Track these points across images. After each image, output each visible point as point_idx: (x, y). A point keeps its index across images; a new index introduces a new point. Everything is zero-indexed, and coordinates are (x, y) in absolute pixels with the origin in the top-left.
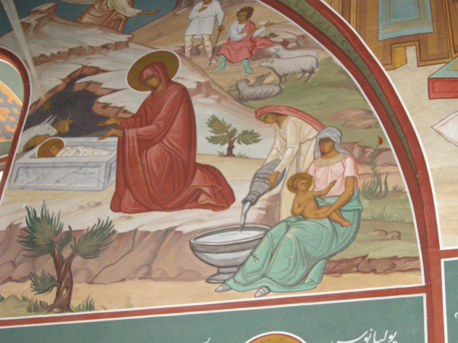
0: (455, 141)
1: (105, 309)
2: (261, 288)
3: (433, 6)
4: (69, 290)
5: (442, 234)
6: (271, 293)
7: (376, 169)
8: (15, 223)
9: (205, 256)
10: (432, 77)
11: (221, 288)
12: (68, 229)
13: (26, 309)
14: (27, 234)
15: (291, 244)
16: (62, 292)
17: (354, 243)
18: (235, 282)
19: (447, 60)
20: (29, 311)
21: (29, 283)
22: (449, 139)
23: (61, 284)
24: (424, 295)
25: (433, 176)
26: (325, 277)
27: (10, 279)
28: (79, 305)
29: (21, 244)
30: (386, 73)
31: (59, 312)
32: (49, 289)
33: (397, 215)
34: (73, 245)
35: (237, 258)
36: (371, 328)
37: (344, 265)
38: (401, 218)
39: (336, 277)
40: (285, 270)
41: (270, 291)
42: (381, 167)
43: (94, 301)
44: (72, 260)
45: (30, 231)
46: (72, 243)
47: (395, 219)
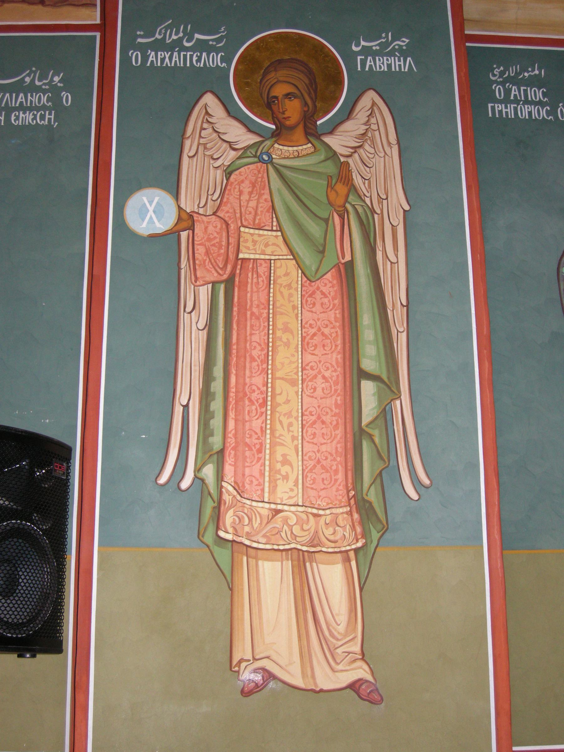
24: (98, 35)
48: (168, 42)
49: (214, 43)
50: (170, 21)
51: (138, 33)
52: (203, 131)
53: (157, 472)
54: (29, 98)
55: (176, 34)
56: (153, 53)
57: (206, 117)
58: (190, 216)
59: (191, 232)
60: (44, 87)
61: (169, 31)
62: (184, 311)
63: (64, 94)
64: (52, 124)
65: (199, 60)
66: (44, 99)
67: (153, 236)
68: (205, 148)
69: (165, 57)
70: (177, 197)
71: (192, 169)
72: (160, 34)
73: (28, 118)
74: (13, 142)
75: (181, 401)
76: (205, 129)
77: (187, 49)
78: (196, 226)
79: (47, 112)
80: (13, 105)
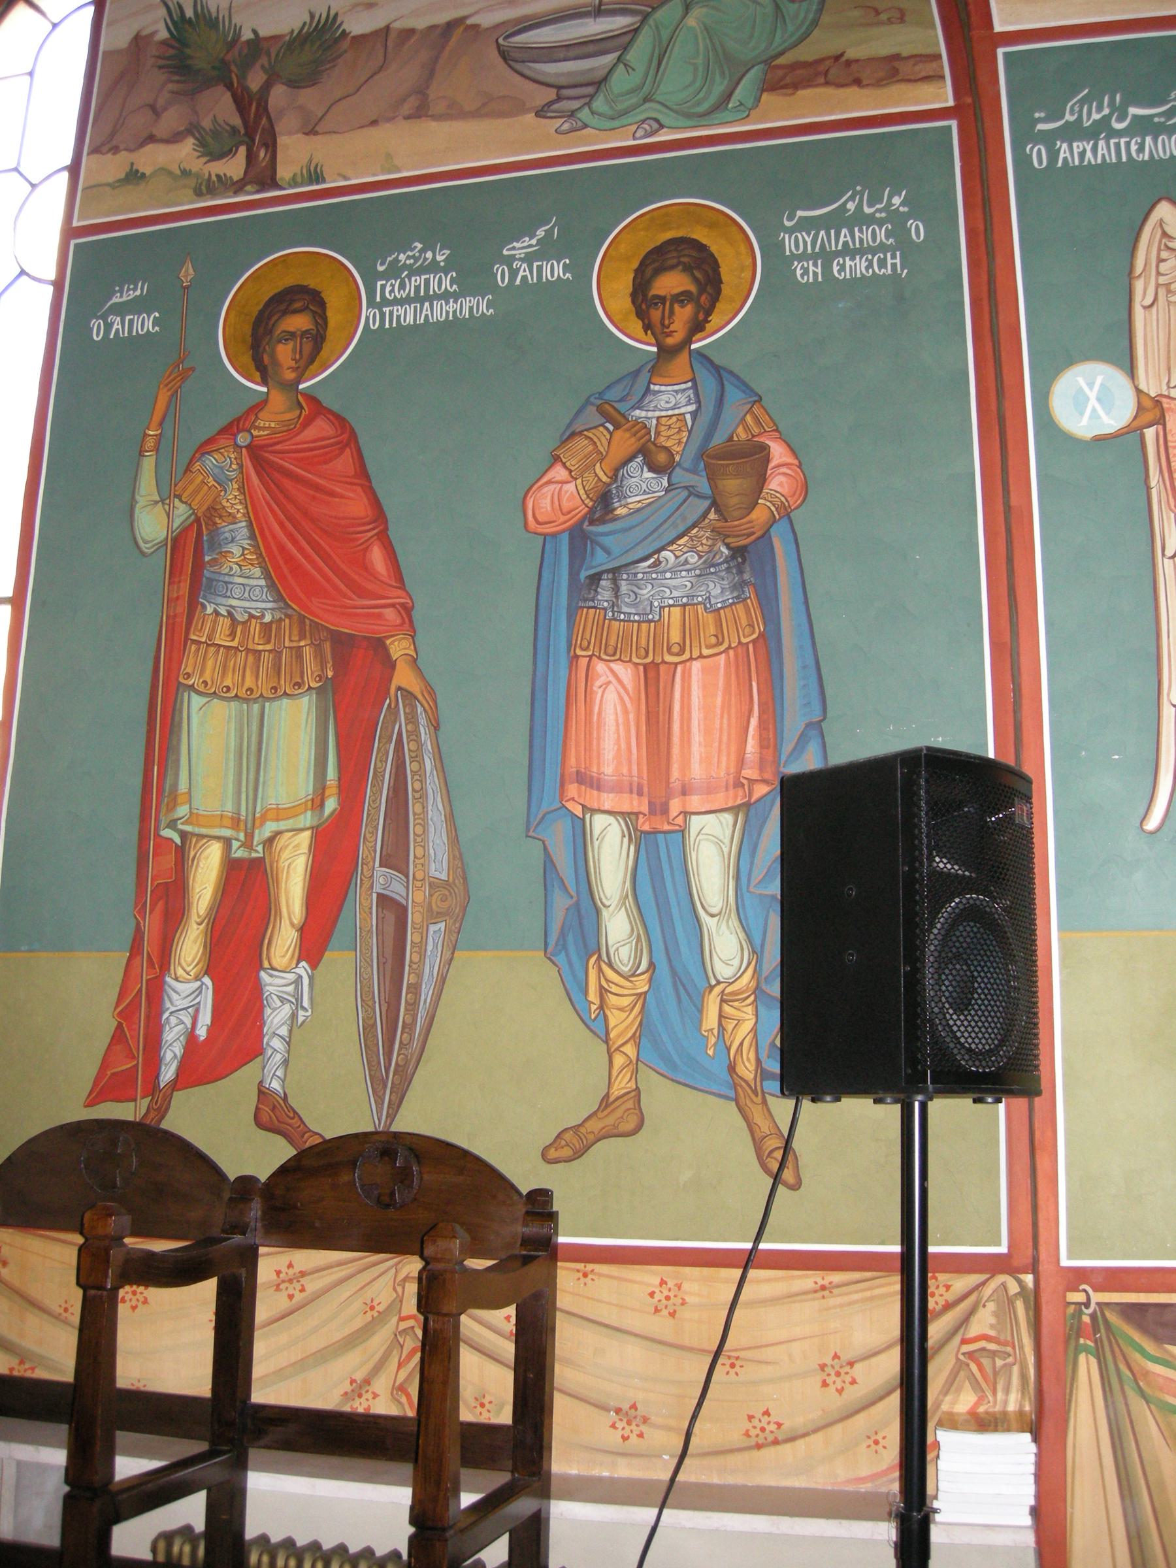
1: (346, 178)
2: (643, 121)
4: (270, 149)
6: (665, 130)
8: (144, 33)
9: (530, 68)
11: (566, 126)
12: (252, 36)
13: (191, 192)
14: (171, 52)
15: (696, 38)
16: (257, 156)
17: (816, 33)
18: (593, 113)
20: (199, 193)
21: (190, 142)
23: (253, 140)
24: (954, 124)
26: (765, 96)
27: (151, 139)
28: (295, 175)
29: (162, 71)
31: (258, 192)
32: (231, 150)
34: (267, 66)
35: (592, 69)
36: (858, 184)
37: (801, 72)
39: (786, 95)
40: (689, 86)
41: (662, 126)
43: (322, 166)
44: (269, 94)
45: (176, 45)
46: (264, 60)
48: (1086, 124)
49: (1162, 120)
50: (1086, 91)
51: (1037, 115)
52: (1162, 265)
53: (1142, 812)
54: (857, 234)
55: (1100, 109)
56: (1065, 146)
57: (1164, 241)
58: (1157, 402)
59: (1160, 427)
60: (878, 215)
61: (1086, 107)
62: (1163, 555)
63: (911, 224)
64: (899, 272)
65: (1141, 149)
66: (881, 235)
67: (1099, 439)
68: (1169, 291)
69: (1084, 151)
70: (1132, 373)
71: (1151, 326)
72: (1072, 112)
73: (858, 266)
74: (840, 306)
75: (1171, 698)
76: (1164, 260)
77: (1119, 134)
78: (1167, 419)
79: (889, 255)
80: (833, 248)
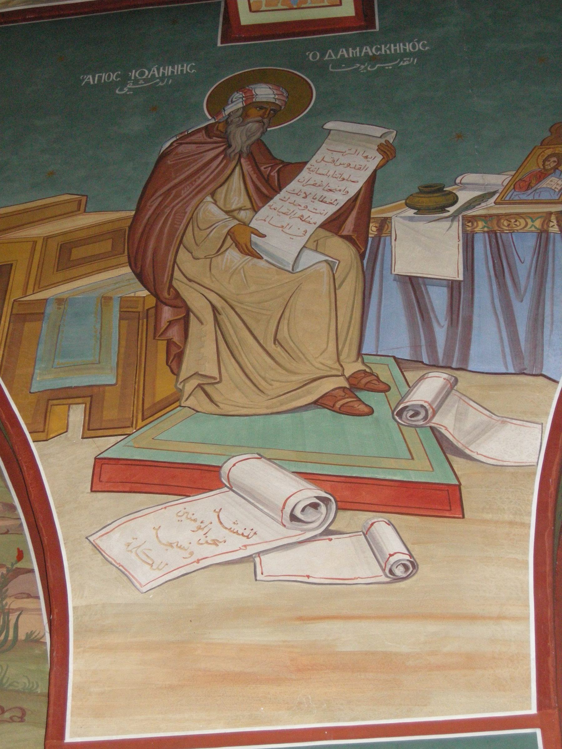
0: (118, 562)
3: (123, 343)
5: (72, 716)
7: (4, 602)
10: (101, 456)
19: (128, 431)
22: (110, 559)
25: (76, 619)
30: (33, 445)
33: (26, 681)
38: (31, 685)
42: (12, 599)
47: (20, 687)
